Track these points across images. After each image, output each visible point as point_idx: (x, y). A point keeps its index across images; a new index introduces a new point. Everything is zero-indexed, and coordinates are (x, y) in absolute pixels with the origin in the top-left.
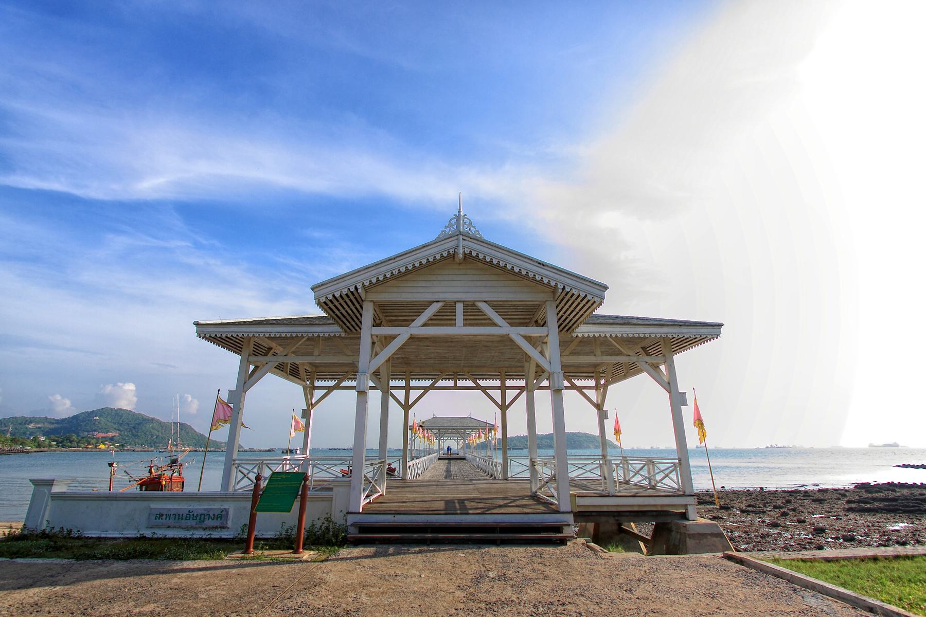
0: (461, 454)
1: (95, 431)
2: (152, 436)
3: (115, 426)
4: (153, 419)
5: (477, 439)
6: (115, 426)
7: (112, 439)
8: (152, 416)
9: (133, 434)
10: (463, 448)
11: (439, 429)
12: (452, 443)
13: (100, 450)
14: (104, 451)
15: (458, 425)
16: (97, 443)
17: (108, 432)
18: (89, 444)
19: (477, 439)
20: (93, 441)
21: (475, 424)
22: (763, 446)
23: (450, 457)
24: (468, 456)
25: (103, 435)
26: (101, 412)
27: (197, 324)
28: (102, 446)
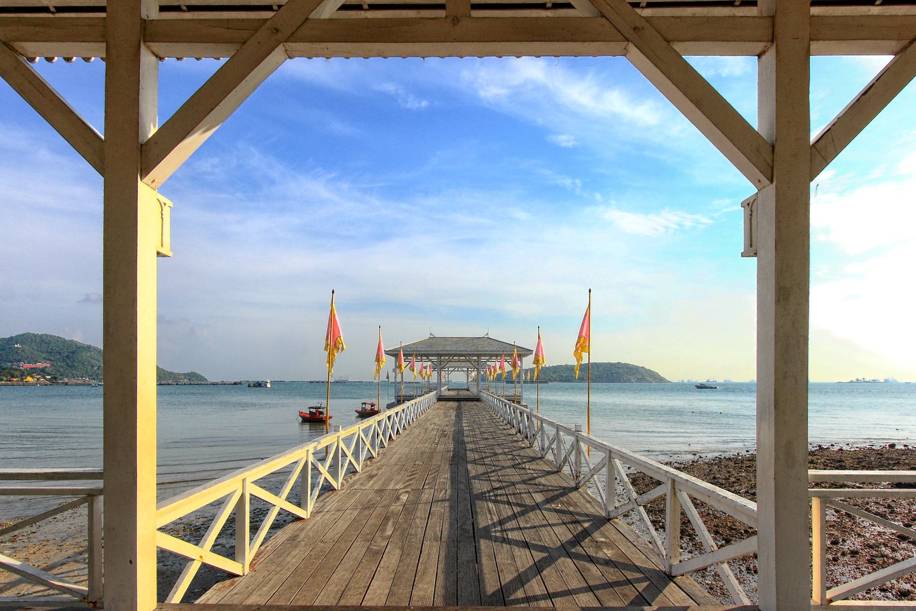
0: (474, 390)
1: (20, 361)
2: (92, 366)
3: (44, 355)
4: (89, 347)
5: (499, 366)
6: (44, 355)
7: (43, 371)
8: (87, 343)
9: (68, 365)
10: (476, 380)
11: (440, 355)
12: (458, 377)
13: (28, 384)
14: (34, 385)
15: (470, 349)
16: (23, 375)
17: (36, 362)
18: (13, 376)
19: (499, 366)
20: (17, 373)
21: (494, 348)
22: (846, 379)
23: (462, 400)
24: (484, 395)
25: (31, 366)
26: (24, 338)
27: (743, 255)
28: (29, 379)
